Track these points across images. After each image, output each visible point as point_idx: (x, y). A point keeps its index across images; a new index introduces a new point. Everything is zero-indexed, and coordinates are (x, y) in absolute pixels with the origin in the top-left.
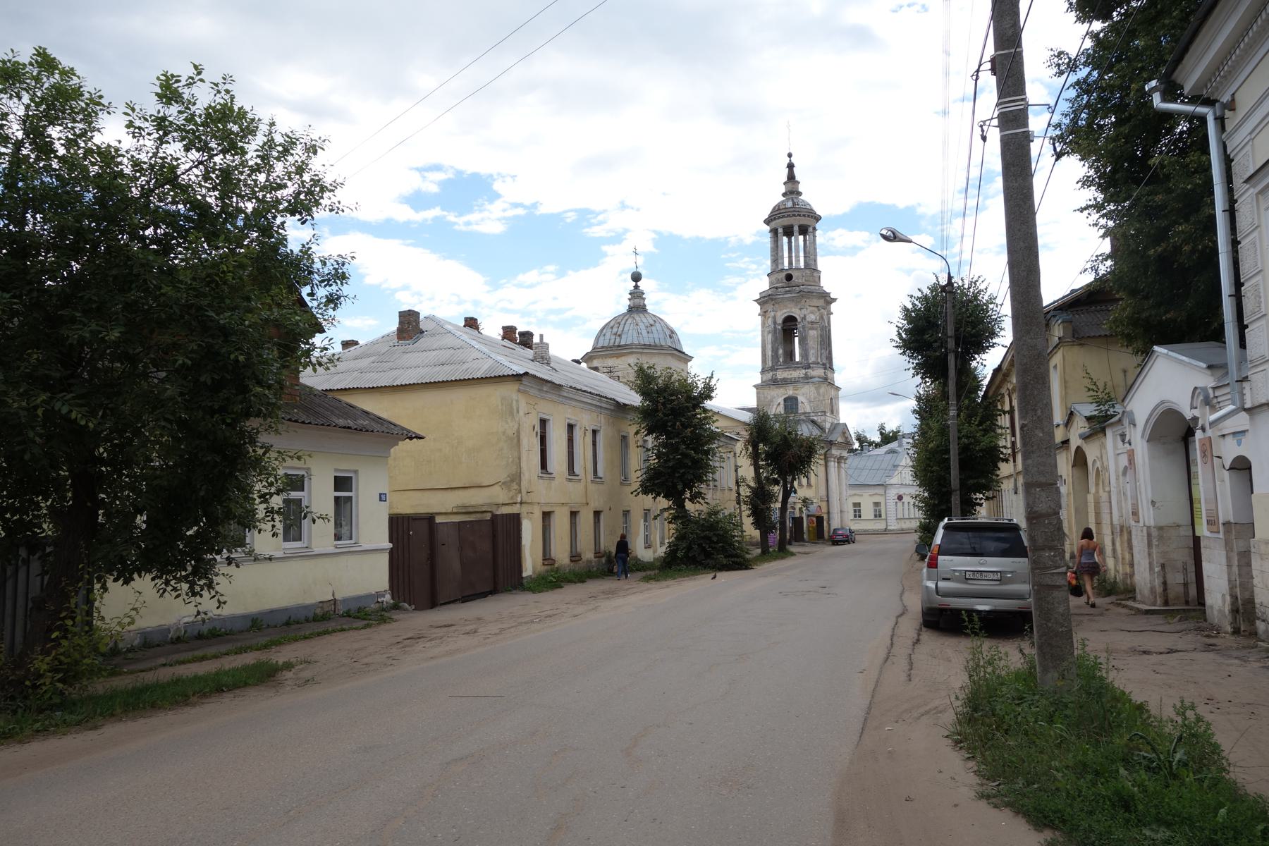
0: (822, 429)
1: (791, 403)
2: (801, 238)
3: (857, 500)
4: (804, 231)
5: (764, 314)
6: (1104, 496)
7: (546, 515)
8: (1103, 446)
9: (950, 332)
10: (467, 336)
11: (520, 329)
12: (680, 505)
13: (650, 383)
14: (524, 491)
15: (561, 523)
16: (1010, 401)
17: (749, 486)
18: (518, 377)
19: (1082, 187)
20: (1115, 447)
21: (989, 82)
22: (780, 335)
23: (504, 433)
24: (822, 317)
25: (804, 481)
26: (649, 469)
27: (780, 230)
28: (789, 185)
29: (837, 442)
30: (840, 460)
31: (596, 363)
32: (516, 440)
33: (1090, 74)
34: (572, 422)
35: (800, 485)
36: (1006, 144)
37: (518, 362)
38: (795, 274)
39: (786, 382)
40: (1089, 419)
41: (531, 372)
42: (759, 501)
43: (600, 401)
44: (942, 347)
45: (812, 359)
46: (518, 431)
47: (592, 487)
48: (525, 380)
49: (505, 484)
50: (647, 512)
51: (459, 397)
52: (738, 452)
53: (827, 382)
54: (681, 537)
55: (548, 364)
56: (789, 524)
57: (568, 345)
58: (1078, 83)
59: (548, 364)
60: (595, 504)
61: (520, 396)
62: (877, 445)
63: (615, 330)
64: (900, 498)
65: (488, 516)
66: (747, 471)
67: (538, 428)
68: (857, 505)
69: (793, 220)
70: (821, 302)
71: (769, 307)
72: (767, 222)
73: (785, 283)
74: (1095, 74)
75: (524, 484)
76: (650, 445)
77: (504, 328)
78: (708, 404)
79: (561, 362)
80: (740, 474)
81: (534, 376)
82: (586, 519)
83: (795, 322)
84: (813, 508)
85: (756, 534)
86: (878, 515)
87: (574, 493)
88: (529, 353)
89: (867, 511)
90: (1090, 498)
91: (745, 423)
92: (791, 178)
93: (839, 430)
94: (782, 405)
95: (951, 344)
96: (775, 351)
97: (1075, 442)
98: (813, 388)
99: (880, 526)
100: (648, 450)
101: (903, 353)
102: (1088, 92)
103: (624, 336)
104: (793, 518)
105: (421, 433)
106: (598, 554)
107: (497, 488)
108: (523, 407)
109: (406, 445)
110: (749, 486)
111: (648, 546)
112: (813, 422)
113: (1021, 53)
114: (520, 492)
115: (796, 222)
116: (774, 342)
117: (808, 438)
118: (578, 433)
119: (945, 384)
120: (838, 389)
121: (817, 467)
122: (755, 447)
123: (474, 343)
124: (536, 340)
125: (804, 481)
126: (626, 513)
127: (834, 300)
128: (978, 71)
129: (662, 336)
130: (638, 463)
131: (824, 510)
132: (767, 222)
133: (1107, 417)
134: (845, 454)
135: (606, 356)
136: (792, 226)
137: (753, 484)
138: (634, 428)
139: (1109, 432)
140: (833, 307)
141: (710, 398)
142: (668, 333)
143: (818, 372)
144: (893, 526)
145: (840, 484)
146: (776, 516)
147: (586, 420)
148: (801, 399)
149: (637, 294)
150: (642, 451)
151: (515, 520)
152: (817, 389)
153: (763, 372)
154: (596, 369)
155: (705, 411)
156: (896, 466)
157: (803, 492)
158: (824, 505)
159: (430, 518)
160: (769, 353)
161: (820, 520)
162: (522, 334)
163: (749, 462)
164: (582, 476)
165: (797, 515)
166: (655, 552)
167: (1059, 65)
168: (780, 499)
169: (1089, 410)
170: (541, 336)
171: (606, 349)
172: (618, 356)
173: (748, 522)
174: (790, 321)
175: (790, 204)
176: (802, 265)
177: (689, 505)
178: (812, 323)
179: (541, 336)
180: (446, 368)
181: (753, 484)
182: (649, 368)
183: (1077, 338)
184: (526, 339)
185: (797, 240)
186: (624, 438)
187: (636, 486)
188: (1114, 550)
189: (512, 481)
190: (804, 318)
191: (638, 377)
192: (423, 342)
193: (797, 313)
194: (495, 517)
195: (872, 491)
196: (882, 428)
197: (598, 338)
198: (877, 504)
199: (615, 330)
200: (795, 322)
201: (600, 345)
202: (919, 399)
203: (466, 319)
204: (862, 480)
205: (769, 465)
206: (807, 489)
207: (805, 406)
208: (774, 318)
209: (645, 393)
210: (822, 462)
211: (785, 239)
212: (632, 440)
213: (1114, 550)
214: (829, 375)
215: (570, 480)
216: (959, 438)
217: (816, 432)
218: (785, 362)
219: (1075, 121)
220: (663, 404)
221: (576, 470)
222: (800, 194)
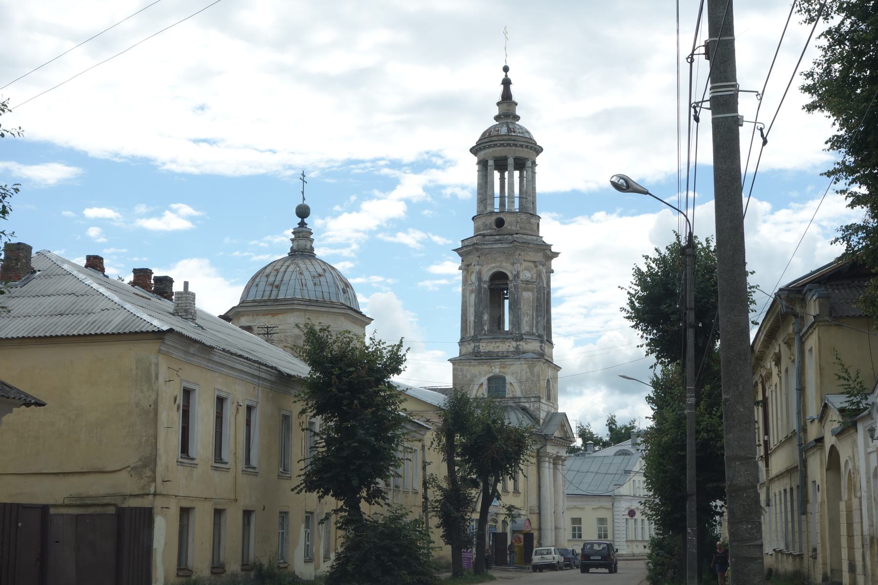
0: (535, 419)
1: (497, 383)
2: (517, 174)
3: (576, 514)
4: (521, 164)
5: (466, 268)
6: (855, 502)
7: (185, 512)
8: (854, 444)
9: (690, 302)
10: (91, 281)
11: (157, 273)
12: (353, 506)
13: (322, 350)
14: (159, 480)
15: (202, 522)
17: (440, 488)
18: (159, 334)
19: (832, 147)
20: (867, 446)
21: (703, 66)
22: (486, 297)
23: (137, 405)
24: (539, 275)
25: (510, 484)
26: (316, 460)
27: (491, 163)
28: (505, 106)
29: (553, 434)
30: (557, 460)
31: (245, 321)
32: (152, 414)
33: (842, 23)
34: (223, 395)
35: (505, 490)
36: (717, 125)
37: (156, 319)
38: (507, 219)
39: (491, 357)
40: (842, 411)
41: (176, 329)
42: (452, 507)
43: (259, 369)
44: (680, 320)
45: (525, 328)
46: (156, 403)
47: (243, 479)
48: (168, 340)
49: (136, 470)
50: (309, 516)
51: (84, 355)
52: (427, 443)
53: (543, 358)
54: (352, 547)
55: (193, 320)
56: (489, 541)
57: (216, 295)
58: (829, 32)
59: (193, 320)
60: (246, 502)
61: (160, 357)
62: (605, 445)
63: (271, 279)
64: (632, 513)
65: (112, 510)
66: (439, 468)
67: (180, 401)
68: (577, 521)
69: (506, 149)
70: (539, 257)
71: (473, 259)
72: (474, 151)
73: (494, 229)
74: (848, 22)
75: (160, 469)
76: (317, 429)
77: (135, 271)
78: (394, 379)
79: (208, 317)
80: (428, 473)
81: (180, 335)
82: (233, 520)
83: (505, 275)
84: (520, 521)
85: (447, 551)
87: (221, 485)
88: (169, 305)
90: (843, 506)
91: (439, 408)
92: (506, 96)
93: (556, 421)
94: (485, 387)
95: (691, 317)
96: (478, 316)
97: (830, 440)
98: (525, 366)
100: (316, 434)
101: (636, 326)
102: (840, 42)
103: (283, 288)
104: (495, 535)
105: (42, 398)
106: (246, 566)
107: (124, 476)
108: (164, 372)
109: (20, 414)
110: (440, 488)
111: (309, 559)
112: (524, 410)
113: (732, 42)
114: (154, 480)
115: (511, 153)
116: (477, 305)
117: (516, 430)
118: (229, 410)
119: (684, 366)
120: (557, 368)
121: (527, 468)
122: (450, 438)
123: (102, 290)
124: (177, 287)
125: (510, 484)
126: (284, 515)
127: (556, 255)
128: (692, 54)
129: (333, 290)
130: (301, 451)
131: (535, 525)
132: (474, 151)
133: (858, 411)
134: (563, 453)
135: (258, 314)
136: (505, 159)
137: (445, 485)
138: (299, 406)
139: (860, 427)
140: (555, 263)
141: (398, 371)
142: (341, 286)
143: (533, 346)
145: (556, 492)
146: (473, 527)
147: (239, 393)
148: (509, 379)
149: (302, 234)
150: (308, 435)
151: (146, 516)
152: (531, 368)
153: (462, 342)
154: (249, 329)
155: (390, 386)
156: (627, 472)
157: (508, 500)
158: (534, 519)
159: (45, 508)
160: (471, 318)
161: (529, 537)
162: (158, 279)
163: (441, 456)
164: (231, 464)
165: (500, 530)
166: (316, 569)
167: (809, 11)
168: (479, 507)
169: (839, 401)
170: (186, 284)
171: (261, 302)
172: (274, 314)
173: (437, 535)
174: (499, 278)
175: (504, 130)
176: (517, 206)
177: (364, 506)
178: (527, 282)
179: (186, 284)
180: (65, 319)
181: (445, 485)
182: (322, 330)
183: (833, 316)
184: (163, 287)
185: (511, 177)
186: (286, 419)
187: (298, 481)
188: (864, 566)
189: (145, 466)
190: (517, 276)
191: (307, 341)
192: (35, 285)
193: (508, 269)
194: (121, 511)
195: (596, 504)
196: (611, 422)
197: (248, 289)
198: (602, 521)
199: (271, 279)
200: (505, 275)
201: (250, 298)
202: (655, 384)
203: (89, 258)
204: (584, 489)
205: (467, 462)
206: (515, 495)
207: (514, 388)
208: (479, 273)
209: (315, 361)
210: (534, 460)
211: (497, 175)
212: (295, 422)
213: (864, 566)
214: (546, 350)
215: (216, 469)
216: (698, 432)
217: (526, 422)
218: (490, 331)
219: (828, 71)
220: (339, 377)
221: (225, 456)
222: (517, 118)
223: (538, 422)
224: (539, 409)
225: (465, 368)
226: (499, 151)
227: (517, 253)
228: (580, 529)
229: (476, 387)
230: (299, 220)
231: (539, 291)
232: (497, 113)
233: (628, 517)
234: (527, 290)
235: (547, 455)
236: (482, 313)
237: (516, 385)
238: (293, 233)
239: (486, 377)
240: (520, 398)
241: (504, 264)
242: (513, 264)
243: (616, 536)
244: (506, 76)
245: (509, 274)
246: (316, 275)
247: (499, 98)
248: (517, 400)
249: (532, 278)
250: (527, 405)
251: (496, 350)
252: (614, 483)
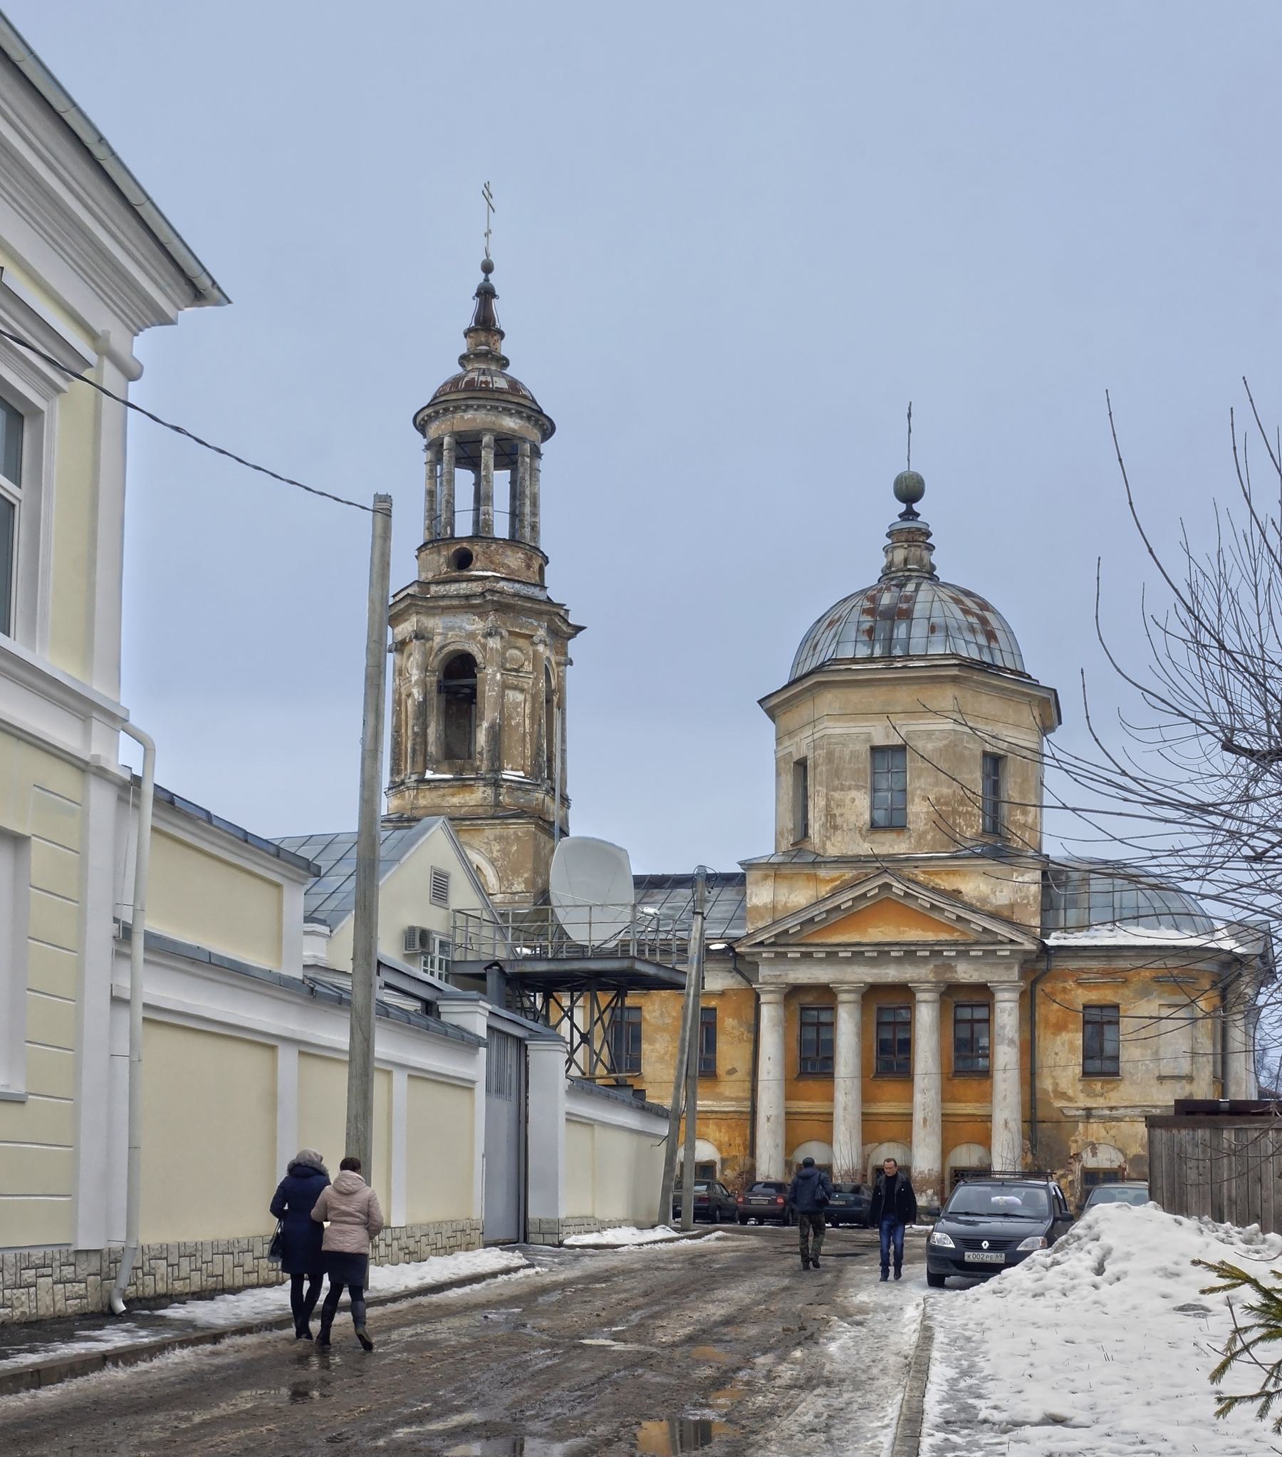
4: (508, 452)
226: (472, 419)
232: (465, 351)
238: (889, 535)
244: (487, 280)
247: (468, 321)
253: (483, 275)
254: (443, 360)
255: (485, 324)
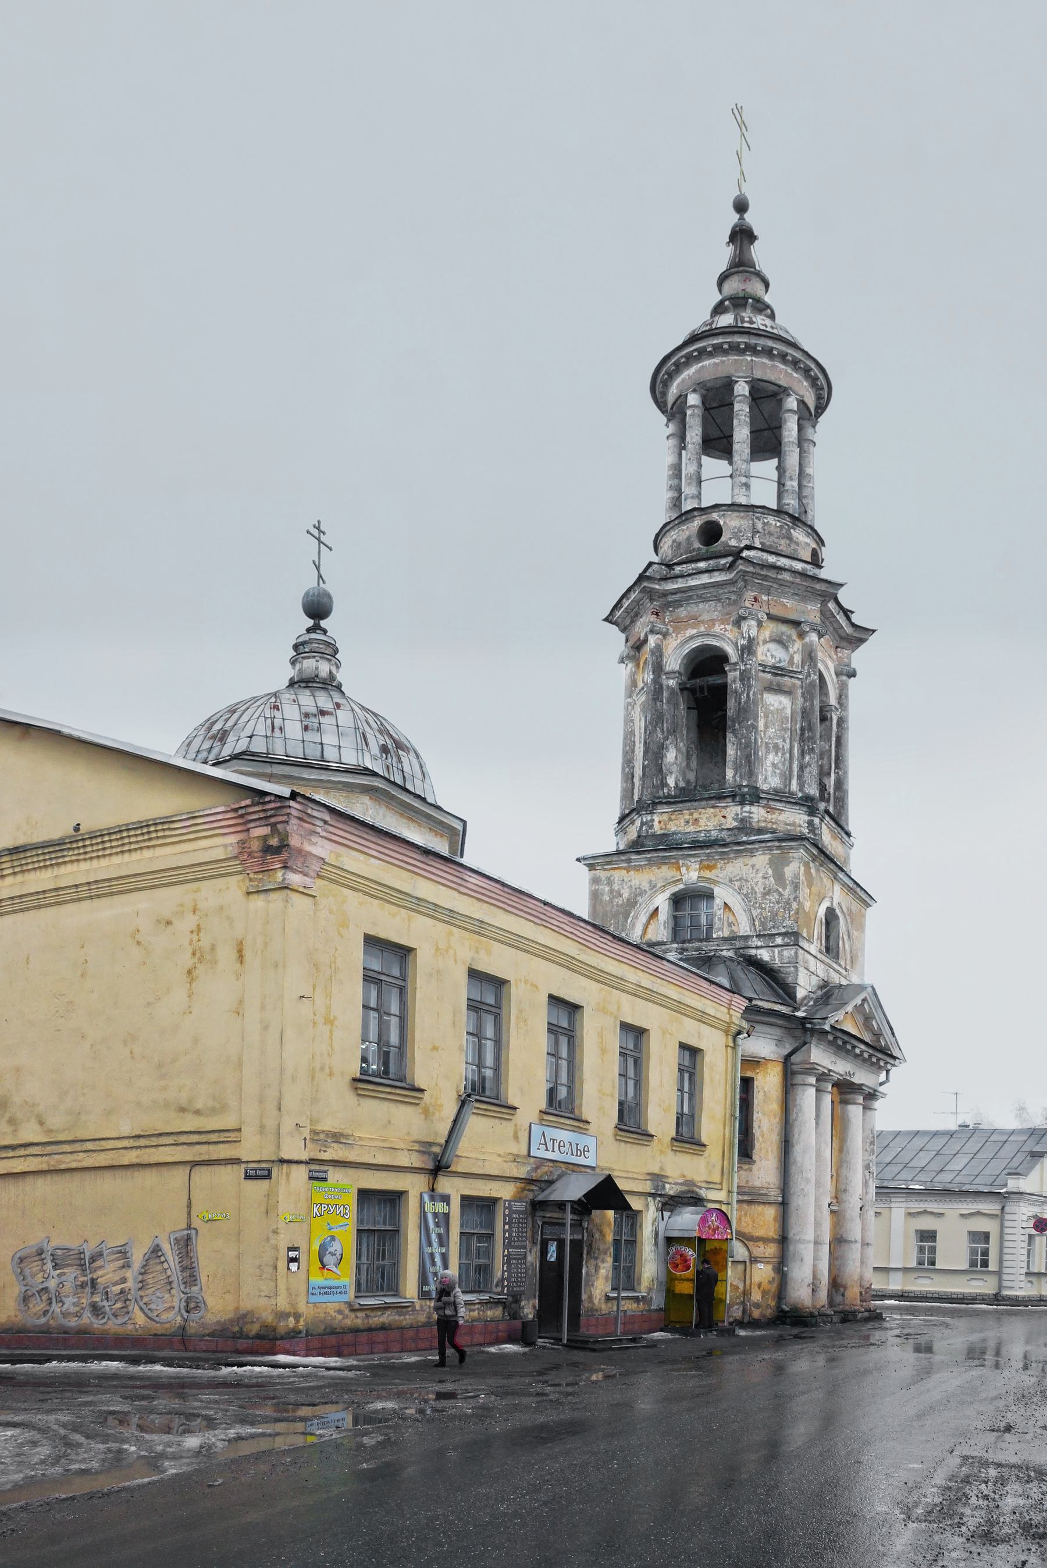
3: (926, 1224)
16: (733, 1340)
38: (731, 523)
68: (927, 1236)
86: (980, 1262)
89: (953, 1251)
94: (664, 914)
99: (983, 1286)
136: (728, 384)
144: (1020, 1288)
148: (722, 894)
174: (707, 664)
178: (778, 671)
223: (792, 995)
224: (794, 962)
225: (617, 875)
227: (750, 595)
228: (933, 1250)
229: (643, 919)
230: (310, 623)
231: (808, 694)
233: (1033, 1232)
234: (778, 690)
235: (810, 1069)
236: (662, 747)
237: (736, 902)
239: (667, 894)
240: (746, 938)
241: (718, 628)
242: (738, 622)
243: (1005, 1264)
245: (730, 650)
246: (314, 710)
248: (739, 944)
249: (791, 661)
250: (764, 955)
251: (691, 829)
252: (1006, 1171)
253: (738, 216)
254: (692, 304)
255: (741, 265)
